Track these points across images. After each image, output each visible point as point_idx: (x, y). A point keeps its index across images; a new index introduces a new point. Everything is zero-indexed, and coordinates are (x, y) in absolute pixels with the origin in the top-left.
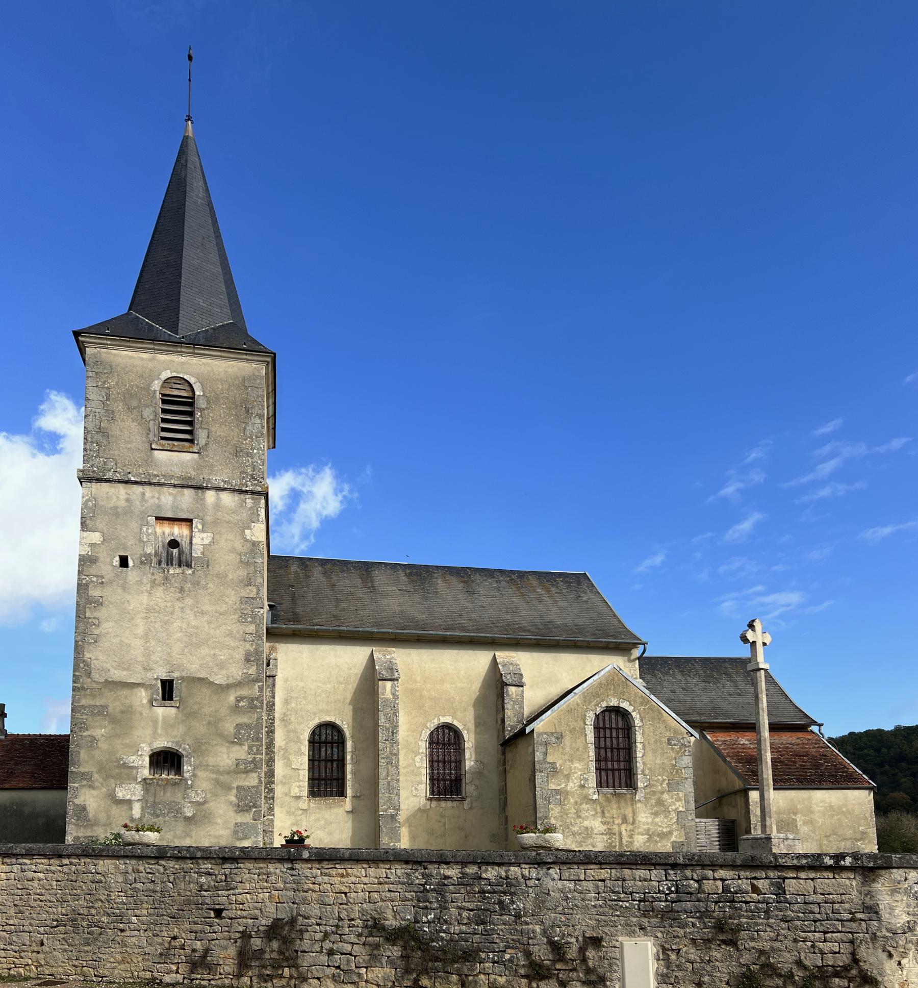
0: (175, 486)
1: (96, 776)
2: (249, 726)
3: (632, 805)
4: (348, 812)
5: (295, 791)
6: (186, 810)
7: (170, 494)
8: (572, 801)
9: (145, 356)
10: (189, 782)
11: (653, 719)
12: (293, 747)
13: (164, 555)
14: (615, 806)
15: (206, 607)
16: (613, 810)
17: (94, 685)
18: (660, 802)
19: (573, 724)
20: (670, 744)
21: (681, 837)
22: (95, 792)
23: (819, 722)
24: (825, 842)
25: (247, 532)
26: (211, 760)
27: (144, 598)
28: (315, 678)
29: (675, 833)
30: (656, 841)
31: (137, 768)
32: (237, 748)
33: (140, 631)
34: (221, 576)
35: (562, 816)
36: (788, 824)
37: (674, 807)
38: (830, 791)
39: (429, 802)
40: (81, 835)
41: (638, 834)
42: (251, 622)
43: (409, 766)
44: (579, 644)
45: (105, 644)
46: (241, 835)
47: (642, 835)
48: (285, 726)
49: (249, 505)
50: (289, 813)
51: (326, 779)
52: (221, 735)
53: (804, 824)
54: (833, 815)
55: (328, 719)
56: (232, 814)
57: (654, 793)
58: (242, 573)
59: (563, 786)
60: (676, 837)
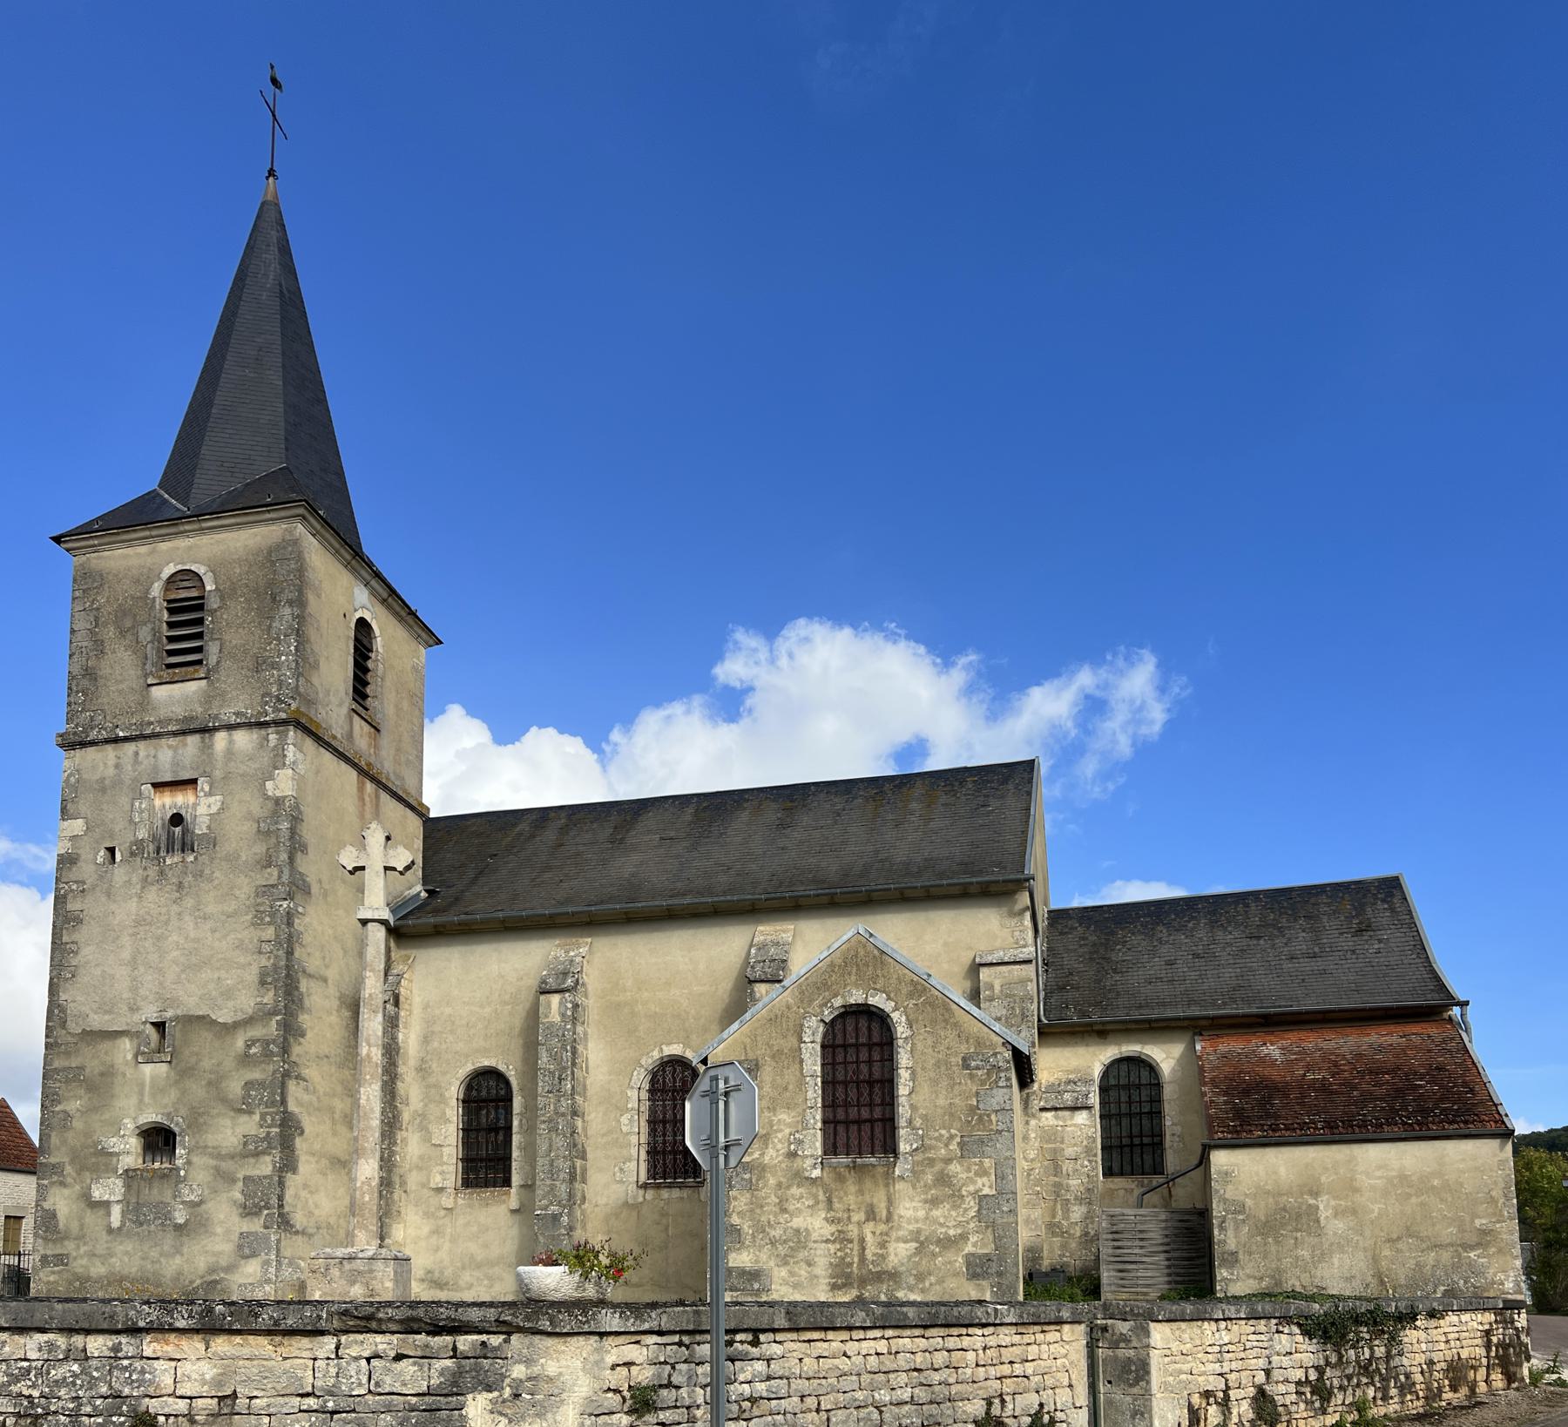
0: (175, 734)
1: (68, 1169)
2: (261, 1084)
3: (887, 1185)
4: (514, 1212)
5: (437, 1180)
6: (177, 1214)
7: (170, 747)
8: (772, 1181)
9: (143, 550)
10: (182, 1173)
11: (934, 1022)
12: (434, 1110)
13: (164, 838)
14: (852, 1188)
15: (211, 908)
16: (850, 1196)
17: (69, 1039)
18: (943, 1180)
19: (778, 1043)
20: (966, 1066)
21: (984, 1245)
22: (66, 1192)
23: (1462, 999)
24: (1387, 1252)
25: (269, 785)
26: (211, 1139)
27: (133, 905)
28: (469, 996)
29: (973, 1239)
30: (934, 1255)
31: (118, 1154)
32: (244, 1118)
33: (126, 954)
34: (232, 859)
35: (752, 1211)
36: (1299, 1216)
37: (971, 1188)
38: (1401, 1145)
39: (641, 1192)
40: (49, 1252)
41: (898, 1240)
42: (269, 924)
43: (610, 1132)
44: (908, 893)
45: (84, 978)
46: (247, 1251)
47: (906, 1242)
48: (424, 1078)
49: (272, 744)
50: (427, 1215)
51: (486, 1159)
52: (224, 1100)
53: (1336, 1215)
54: (1409, 1196)
55: (486, 1063)
56: (236, 1219)
57: (931, 1162)
58: (260, 849)
59: (756, 1155)
60: (975, 1245)
